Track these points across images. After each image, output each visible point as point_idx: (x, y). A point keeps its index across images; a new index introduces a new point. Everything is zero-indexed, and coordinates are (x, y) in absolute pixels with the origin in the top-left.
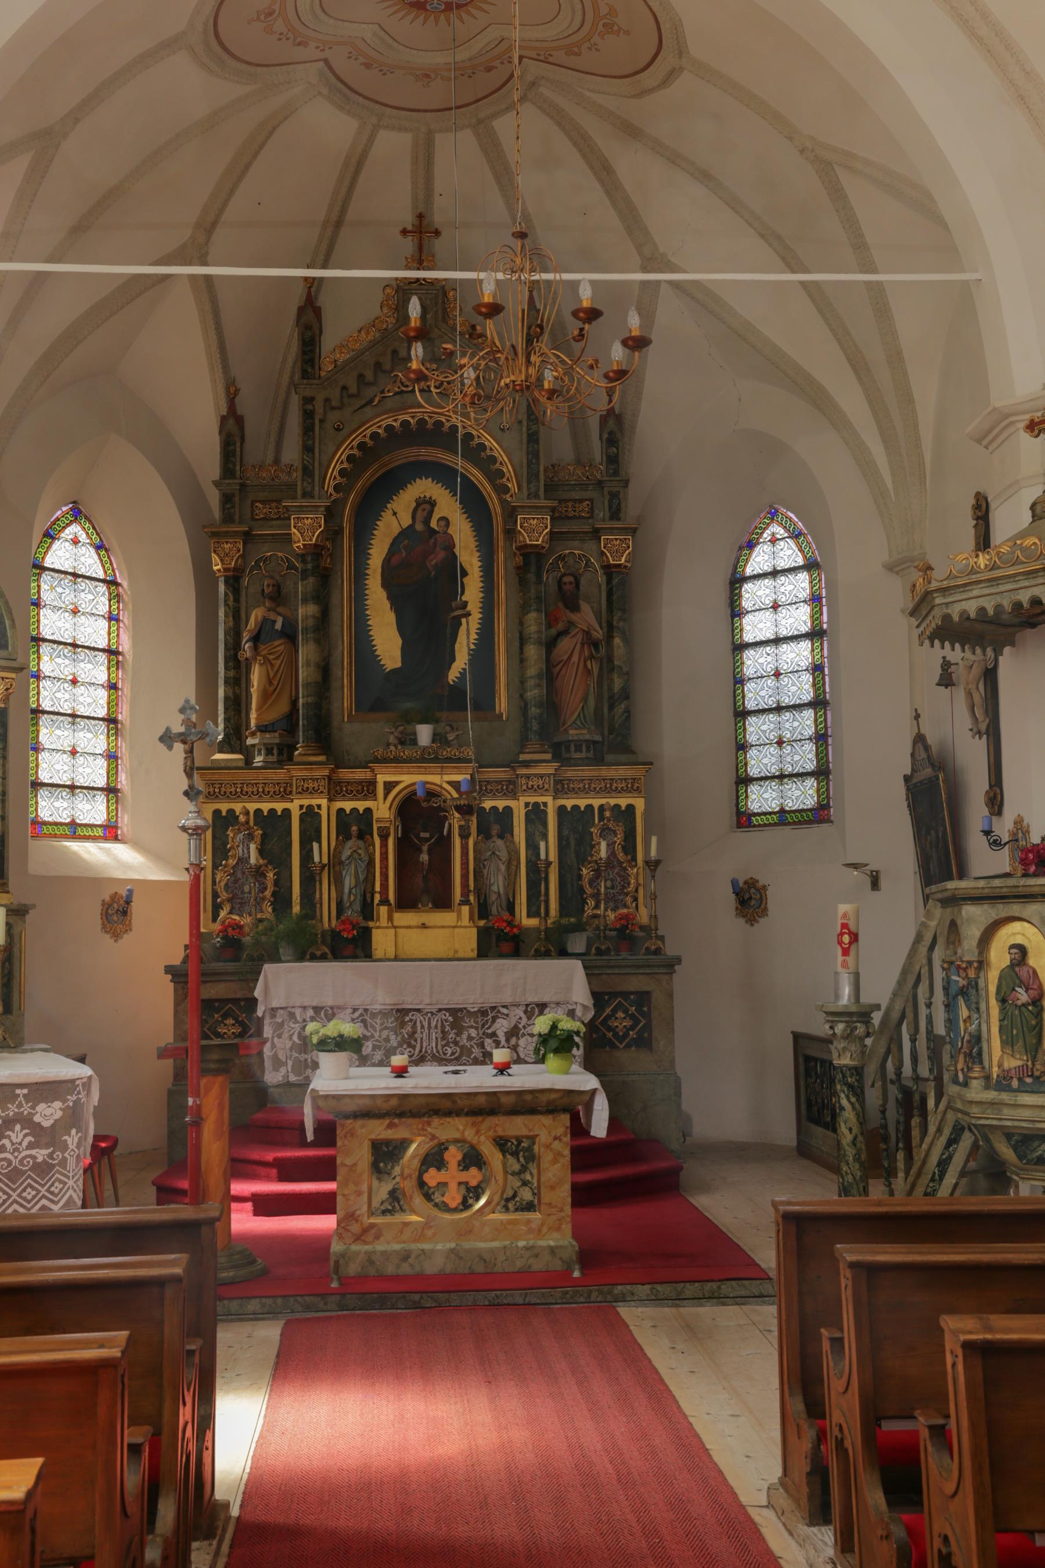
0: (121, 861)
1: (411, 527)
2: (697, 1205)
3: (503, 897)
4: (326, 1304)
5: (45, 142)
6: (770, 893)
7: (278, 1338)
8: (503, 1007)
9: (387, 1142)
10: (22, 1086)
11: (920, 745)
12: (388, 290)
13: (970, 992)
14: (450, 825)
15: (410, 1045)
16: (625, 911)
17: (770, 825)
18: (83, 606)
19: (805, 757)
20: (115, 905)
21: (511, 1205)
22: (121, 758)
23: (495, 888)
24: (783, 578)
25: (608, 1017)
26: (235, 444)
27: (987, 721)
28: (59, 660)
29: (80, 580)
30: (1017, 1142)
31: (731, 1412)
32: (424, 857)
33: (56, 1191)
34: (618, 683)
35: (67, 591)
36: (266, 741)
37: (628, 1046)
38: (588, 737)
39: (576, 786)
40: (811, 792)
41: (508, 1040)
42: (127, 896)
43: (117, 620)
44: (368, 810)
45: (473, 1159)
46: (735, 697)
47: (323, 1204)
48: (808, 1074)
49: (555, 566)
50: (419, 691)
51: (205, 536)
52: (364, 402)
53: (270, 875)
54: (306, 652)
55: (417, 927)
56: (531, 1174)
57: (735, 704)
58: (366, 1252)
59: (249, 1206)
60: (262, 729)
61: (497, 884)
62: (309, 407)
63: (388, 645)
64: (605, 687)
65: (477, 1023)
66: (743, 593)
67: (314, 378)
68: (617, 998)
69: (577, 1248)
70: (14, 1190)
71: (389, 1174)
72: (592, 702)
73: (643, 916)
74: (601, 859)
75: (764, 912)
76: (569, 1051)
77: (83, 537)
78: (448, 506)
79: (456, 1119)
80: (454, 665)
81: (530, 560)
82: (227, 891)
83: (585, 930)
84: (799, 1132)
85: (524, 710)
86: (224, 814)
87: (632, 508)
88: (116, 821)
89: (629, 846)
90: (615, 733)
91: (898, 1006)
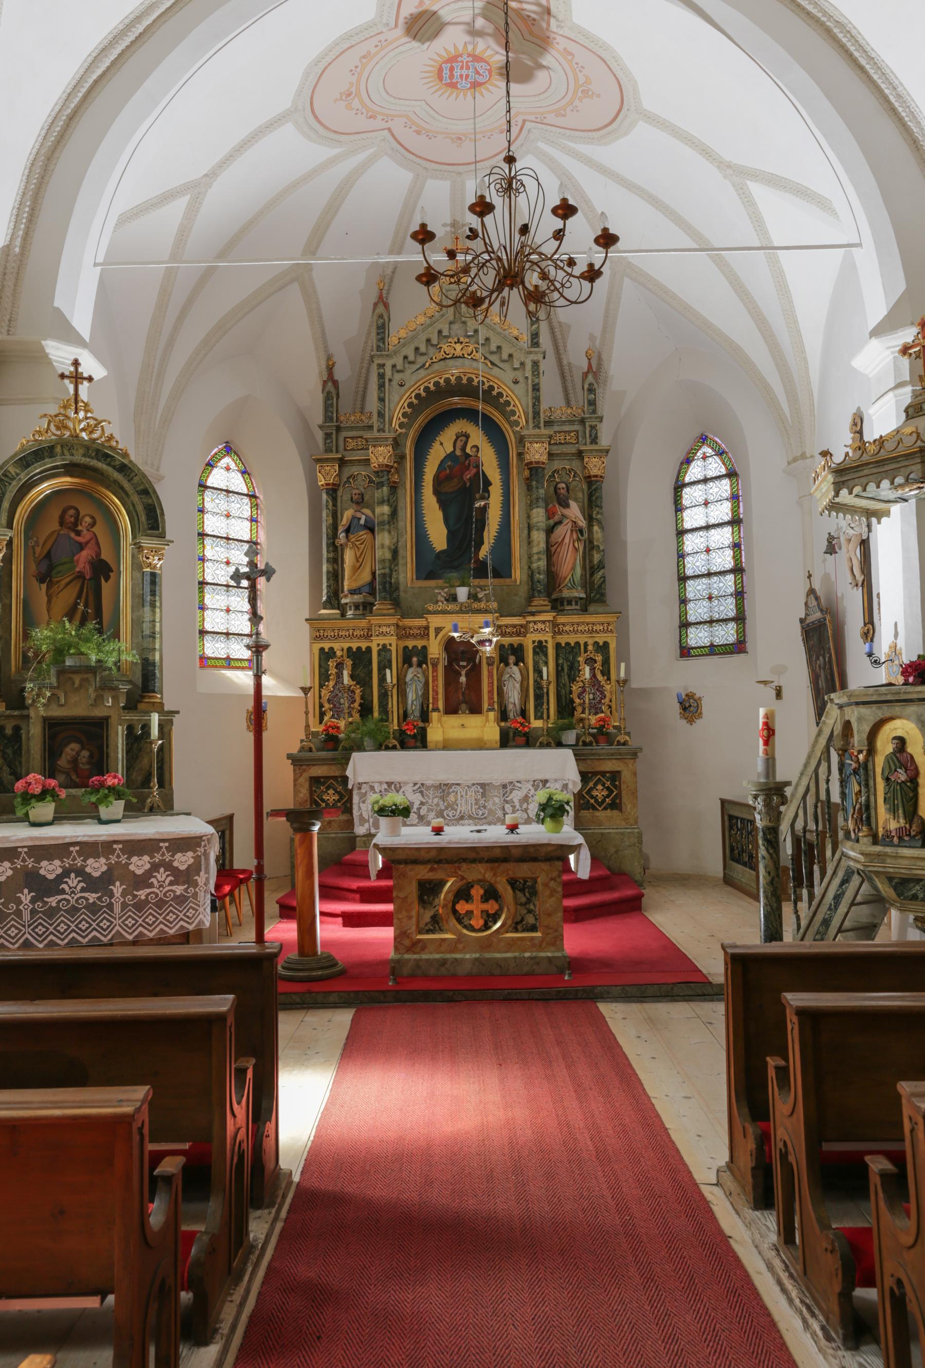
7: (350, 1022)
9: (430, 882)
10: (164, 841)
11: (812, 596)
13: (864, 771)
19: (728, 608)
21: (519, 927)
23: (511, 700)
25: (591, 789)
28: (217, 549)
30: (897, 883)
31: (684, 1095)
32: (463, 679)
34: (597, 557)
35: (222, 502)
37: (605, 809)
39: (567, 628)
40: (732, 632)
43: (257, 521)
44: (424, 648)
45: (491, 894)
47: (382, 920)
48: (731, 828)
53: (358, 691)
56: (534, 905)
58: (415, 960)
59: (340, 920)
60: (353, 592)
61: (513, 696)
62: (382, 371)
70: (160, 915)
72: (579, 571)
75: (700, 715)
77: (233, 466)
78: (477, 437)
80: (483, 547)
81: (534, 471)
84: (725, 869)
86: (327, 650)
87: (604, 441)
89: (606, 672)
90: (597, 591)
91: (804, 782)
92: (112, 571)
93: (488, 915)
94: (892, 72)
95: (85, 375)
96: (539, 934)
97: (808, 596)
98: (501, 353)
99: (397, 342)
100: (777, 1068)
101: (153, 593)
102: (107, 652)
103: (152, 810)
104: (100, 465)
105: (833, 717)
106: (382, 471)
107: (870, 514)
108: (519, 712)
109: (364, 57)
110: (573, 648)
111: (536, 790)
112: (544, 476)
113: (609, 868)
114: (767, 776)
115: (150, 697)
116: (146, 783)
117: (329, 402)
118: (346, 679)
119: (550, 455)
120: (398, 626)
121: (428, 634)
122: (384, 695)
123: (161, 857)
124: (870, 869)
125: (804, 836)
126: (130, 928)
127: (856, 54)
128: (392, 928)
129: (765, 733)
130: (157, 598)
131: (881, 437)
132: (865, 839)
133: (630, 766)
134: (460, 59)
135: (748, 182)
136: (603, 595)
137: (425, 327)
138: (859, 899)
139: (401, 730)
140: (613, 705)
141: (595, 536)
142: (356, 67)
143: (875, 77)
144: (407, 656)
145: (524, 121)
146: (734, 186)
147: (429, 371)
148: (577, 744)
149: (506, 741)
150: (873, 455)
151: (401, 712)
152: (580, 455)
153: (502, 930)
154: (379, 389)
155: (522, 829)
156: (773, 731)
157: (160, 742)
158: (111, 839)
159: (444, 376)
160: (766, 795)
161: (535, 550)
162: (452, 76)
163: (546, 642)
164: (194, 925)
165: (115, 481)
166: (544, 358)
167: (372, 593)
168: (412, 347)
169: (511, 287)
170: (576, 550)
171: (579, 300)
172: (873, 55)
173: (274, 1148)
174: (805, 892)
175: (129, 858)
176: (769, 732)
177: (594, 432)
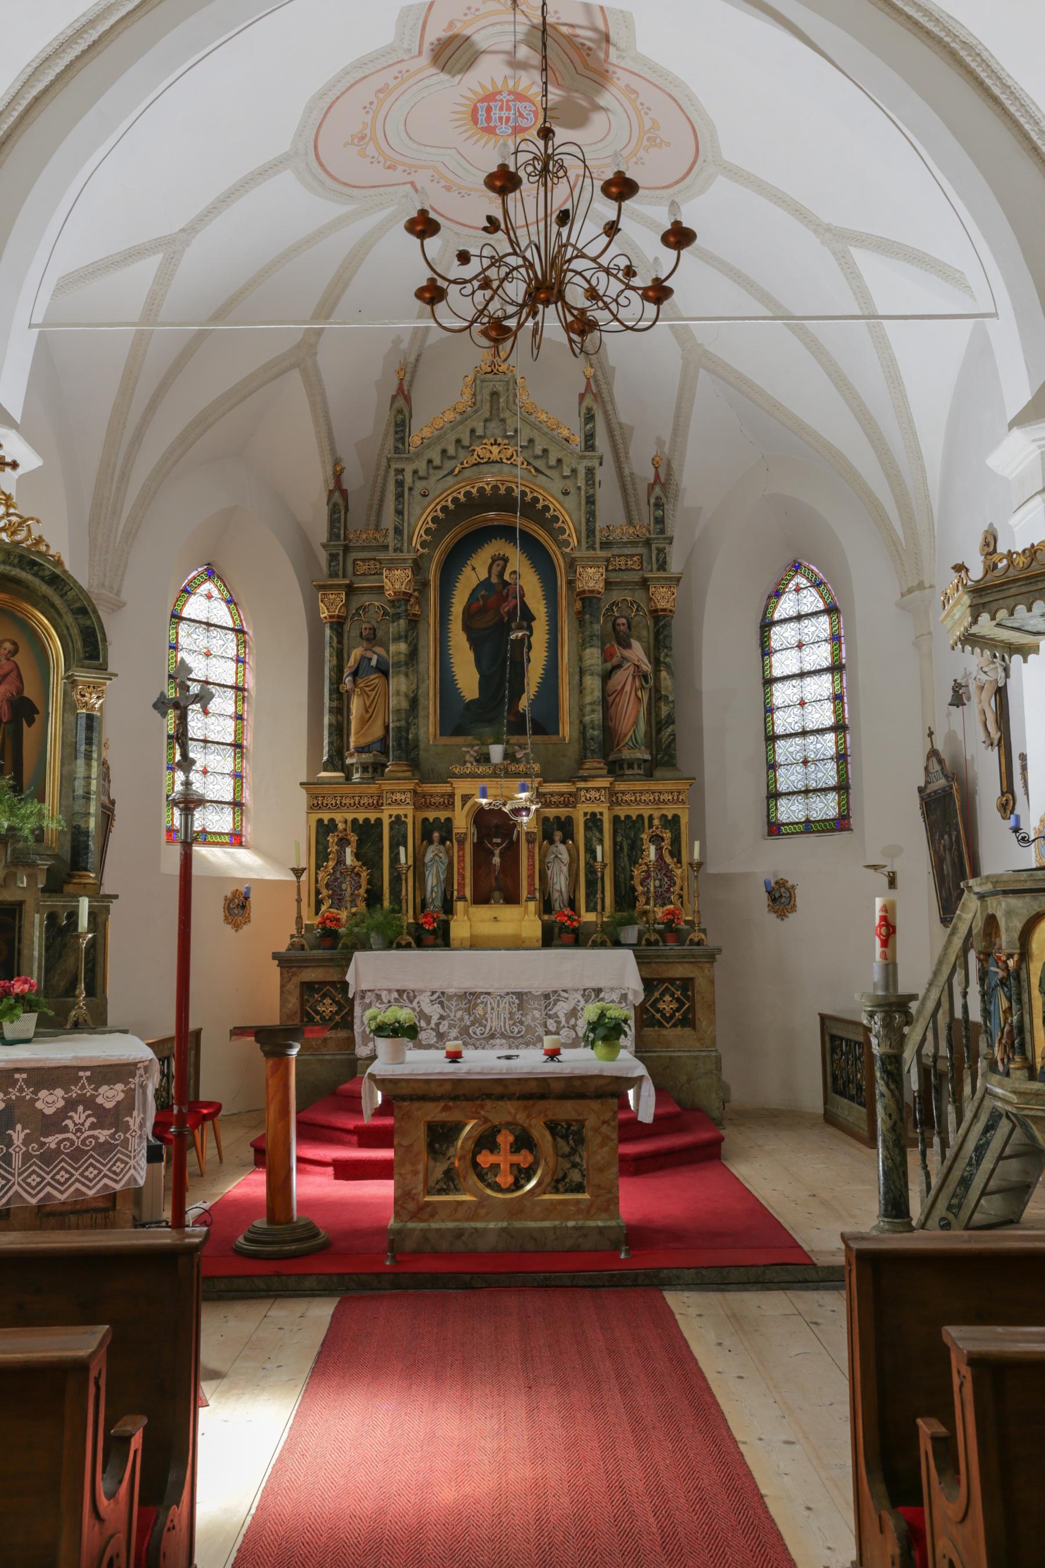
0: (244, 864)
2: (738, 1176)
6: (798, 891)
7: (329, 1319)
9: (443, 1124)
10: (84, 1069)
11: (934, 759)
19: (828, 775)
21: (560, 1186)
23: (557, 887)
25: (657, 1000)
27: (999, 734)
31: (784, 1438)
32: (496, 860)
33: (118, 1171)
34: (665, 710)
35: (201, 637)
37: (674, 1026)
39: (627, 797)
40: (833, 804)
41: (567, 1022)
43: (244, 662)
44: (449, 820)
45: (524, 1142)
46: (765, 724)
48: (833, 1051)
51: (316, 588)
52: (445, 472)
53: (364, 874)
56: (580, 1156)
57: (766, 729)
58: (421, 1230)
59: (330, 1170)
60: (360, 750)
61: (560, 882)
62: (400, 477)
63: (468, 681)
64: (653, 715)
70: (76, 1170)
72: (642, 726)
75: (793, 908)
77: (215, 593)
78: (518, 563)
81: (588, 602)
84: (825, 1103)
85: (583, 732)
86: (326, 822)
87: (675, 566)
89: (676, 853)
90: (665, 750)
91: (934, 995)
92: (37, 712)
93: (520, 1170)
94: (1034, 103)
95: (8, 460)
96: (586, 1196)
97: (928, 758)
98: (547, 458)
99: (419, 443)
100: (935, 1439)
101: (89, 741)
102: (23, 817)
103: (78, 1027)
104: (24, 575)
105: (970, 912)
106: (399, 600)
107: (1014, 649)
108: (566, 902)
109: (380, 91)
110: (635, 822)
111: (587, 1001)
112: (599, 608)
113: (679, 1103)
114: (886, 987)
115: (81, 877)
116: (70, 990)
117: (336, 516)
118: (349, 859)
119: (608, 584)
120: (415, 792)
121: (453, 803)
122: (396, 880)
123: (24, 1109)
124: (1026, 1112)
125: (935, 1066)
126: (34, 1188)
127: (988, 82)
128: (392, 1182)
129: (883, 930)
130: (94, 748)
131: (1033, 545)
132: (1019, 1073)
133: (706, 971)
134: (498, 97)
135: (852, 249)
136: (672, 757)
137: (454, 425)
138: (1008, 1151)
139: (417, 924)
140: (685, 893)
141: (663, 684)
142: (371, 103)
143: (1012, 109)
144: (426, 831)
146: (834, 254)
147: (459, 478)
148: (639, 944)
149: (549, 939)
150: (1023, 569)
151: (418, 900)
152: (644, 583)
153: (537, 1191)
154: (396, 499)
155: (566, 1054)
156: (894, 928)
157: (90, 936)
158: (11, 1066)
159: (478, 485)
160: (885, 1012)
161: (588, 699)
162: (489, 119)
163: (601, 814)
164: (123, 1183)
165: (44, 597)
166: (601, 464)
167: (385, 752)
168: (439, 448)
169: (546, 303)
170: (639, 700)
172: (1010, 83)
173: (185, 1542)
174: (936, 1140)
175: (35, 1093)
176: (889, 929)
177: (662, 556)
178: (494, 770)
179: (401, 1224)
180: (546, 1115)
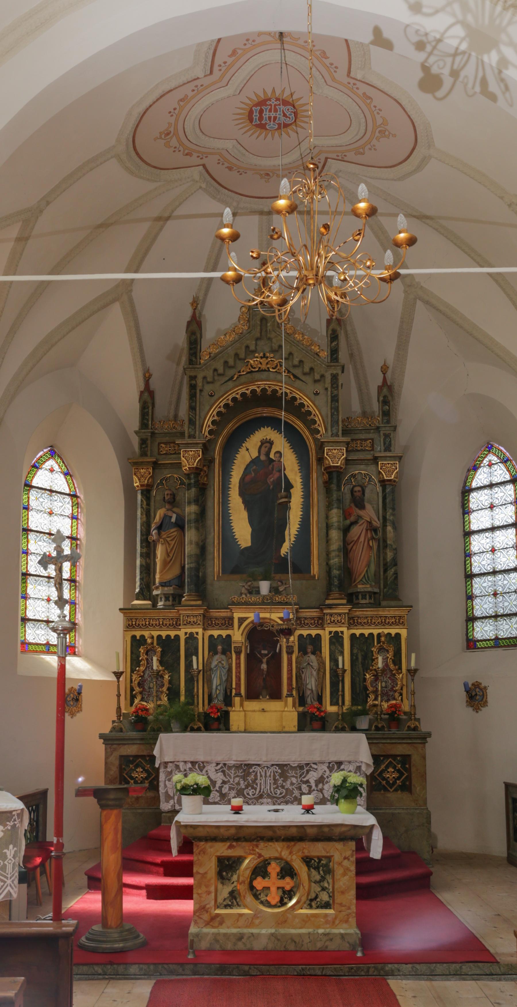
1: (258, 458)
2: (442, 900)
3: (315, 692)
4: (183, 970)
5: (29, 218)
7: (148, 995)
8: (314, 763)
9: (229, 858)
12: (244, 309)
14: (281, 646)
15: (253, 788)
16: (394, 702)
17: (489, 647)
18: (56, 510)
20: (72, 695)
22: (78, 604)
24: (496, 489)
25: (383, 771)
26: (148, 408)
28: (40, 543)
29: (54, 494)
32: (264, 666)
34: (390, 555)
35: (46, 501)
36: (165, 592)
37: (396, 790)
38: (370, 589)
41: (317, 786)
42: (79, 689)
43: (77, 519)
44: (229, 636)
45: (287, 871)
47: (185, 893)
49: (349, 481)
50: (262, 559)
51: (131, 464)
52: (227, 378)
53: (166, 677)
54: (191, 535)
55: (259, 711)
56: (328, 882)
57: (465, 569)
58: (213, 934)
59: (144, 892)
60: (163, 584)
61: (311, 683)
62: (193, 382)
63: (243, 532)
64: (382, 558)
65: (297, 774)
66: (471, 499)
67: (197, 364)
68: (388, 758)
69: (360, 936)
71: (229, 880)
72: (373, 567)
73: (406, 707)
74: (378, 668)
75: (485, 704)
76: (355, 798)
77: (56, 468)
78: (280, 443)
79: (276, 843)
81: (333, 477)
82: (139, 687)
83: (368, 714)
86: (138, 638)
88: (75, 643)
89: (397, 660)
90: (388, 586)
93: (284, 892)
96: (331, 911)
98: (303, 367)
109: (181, 100)
111: (331, 771)
128: (192, 901)
134: (268, 103)
142: (175, 109)
145: (326, 159)
153: (296, 907)
162: (261, 118)
166: (343, 372)
167: (181, 585)
168: (222, 361)
171: (376, 301)
178: (263, 600)
179: (198, 930)
180: (303, 852)
